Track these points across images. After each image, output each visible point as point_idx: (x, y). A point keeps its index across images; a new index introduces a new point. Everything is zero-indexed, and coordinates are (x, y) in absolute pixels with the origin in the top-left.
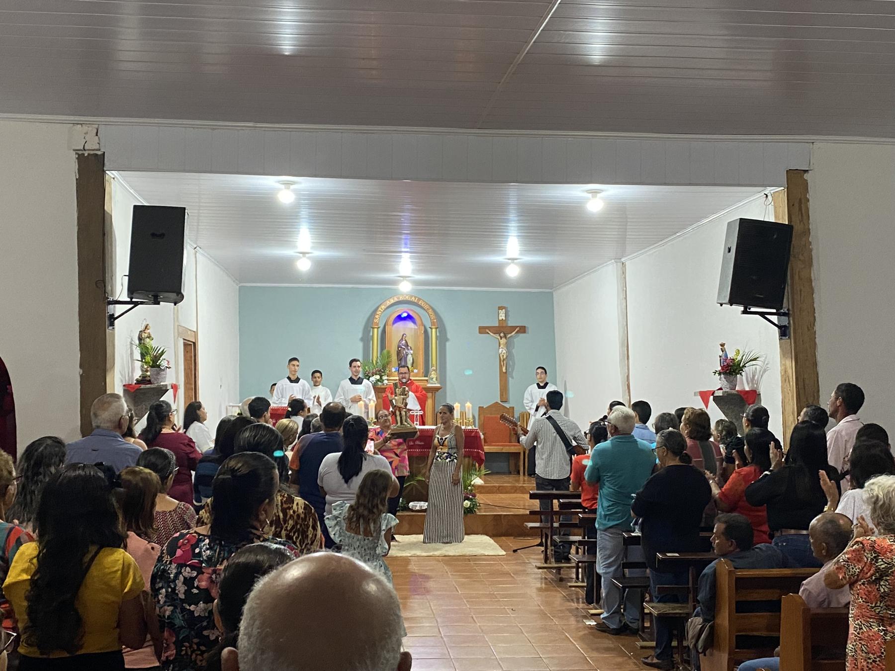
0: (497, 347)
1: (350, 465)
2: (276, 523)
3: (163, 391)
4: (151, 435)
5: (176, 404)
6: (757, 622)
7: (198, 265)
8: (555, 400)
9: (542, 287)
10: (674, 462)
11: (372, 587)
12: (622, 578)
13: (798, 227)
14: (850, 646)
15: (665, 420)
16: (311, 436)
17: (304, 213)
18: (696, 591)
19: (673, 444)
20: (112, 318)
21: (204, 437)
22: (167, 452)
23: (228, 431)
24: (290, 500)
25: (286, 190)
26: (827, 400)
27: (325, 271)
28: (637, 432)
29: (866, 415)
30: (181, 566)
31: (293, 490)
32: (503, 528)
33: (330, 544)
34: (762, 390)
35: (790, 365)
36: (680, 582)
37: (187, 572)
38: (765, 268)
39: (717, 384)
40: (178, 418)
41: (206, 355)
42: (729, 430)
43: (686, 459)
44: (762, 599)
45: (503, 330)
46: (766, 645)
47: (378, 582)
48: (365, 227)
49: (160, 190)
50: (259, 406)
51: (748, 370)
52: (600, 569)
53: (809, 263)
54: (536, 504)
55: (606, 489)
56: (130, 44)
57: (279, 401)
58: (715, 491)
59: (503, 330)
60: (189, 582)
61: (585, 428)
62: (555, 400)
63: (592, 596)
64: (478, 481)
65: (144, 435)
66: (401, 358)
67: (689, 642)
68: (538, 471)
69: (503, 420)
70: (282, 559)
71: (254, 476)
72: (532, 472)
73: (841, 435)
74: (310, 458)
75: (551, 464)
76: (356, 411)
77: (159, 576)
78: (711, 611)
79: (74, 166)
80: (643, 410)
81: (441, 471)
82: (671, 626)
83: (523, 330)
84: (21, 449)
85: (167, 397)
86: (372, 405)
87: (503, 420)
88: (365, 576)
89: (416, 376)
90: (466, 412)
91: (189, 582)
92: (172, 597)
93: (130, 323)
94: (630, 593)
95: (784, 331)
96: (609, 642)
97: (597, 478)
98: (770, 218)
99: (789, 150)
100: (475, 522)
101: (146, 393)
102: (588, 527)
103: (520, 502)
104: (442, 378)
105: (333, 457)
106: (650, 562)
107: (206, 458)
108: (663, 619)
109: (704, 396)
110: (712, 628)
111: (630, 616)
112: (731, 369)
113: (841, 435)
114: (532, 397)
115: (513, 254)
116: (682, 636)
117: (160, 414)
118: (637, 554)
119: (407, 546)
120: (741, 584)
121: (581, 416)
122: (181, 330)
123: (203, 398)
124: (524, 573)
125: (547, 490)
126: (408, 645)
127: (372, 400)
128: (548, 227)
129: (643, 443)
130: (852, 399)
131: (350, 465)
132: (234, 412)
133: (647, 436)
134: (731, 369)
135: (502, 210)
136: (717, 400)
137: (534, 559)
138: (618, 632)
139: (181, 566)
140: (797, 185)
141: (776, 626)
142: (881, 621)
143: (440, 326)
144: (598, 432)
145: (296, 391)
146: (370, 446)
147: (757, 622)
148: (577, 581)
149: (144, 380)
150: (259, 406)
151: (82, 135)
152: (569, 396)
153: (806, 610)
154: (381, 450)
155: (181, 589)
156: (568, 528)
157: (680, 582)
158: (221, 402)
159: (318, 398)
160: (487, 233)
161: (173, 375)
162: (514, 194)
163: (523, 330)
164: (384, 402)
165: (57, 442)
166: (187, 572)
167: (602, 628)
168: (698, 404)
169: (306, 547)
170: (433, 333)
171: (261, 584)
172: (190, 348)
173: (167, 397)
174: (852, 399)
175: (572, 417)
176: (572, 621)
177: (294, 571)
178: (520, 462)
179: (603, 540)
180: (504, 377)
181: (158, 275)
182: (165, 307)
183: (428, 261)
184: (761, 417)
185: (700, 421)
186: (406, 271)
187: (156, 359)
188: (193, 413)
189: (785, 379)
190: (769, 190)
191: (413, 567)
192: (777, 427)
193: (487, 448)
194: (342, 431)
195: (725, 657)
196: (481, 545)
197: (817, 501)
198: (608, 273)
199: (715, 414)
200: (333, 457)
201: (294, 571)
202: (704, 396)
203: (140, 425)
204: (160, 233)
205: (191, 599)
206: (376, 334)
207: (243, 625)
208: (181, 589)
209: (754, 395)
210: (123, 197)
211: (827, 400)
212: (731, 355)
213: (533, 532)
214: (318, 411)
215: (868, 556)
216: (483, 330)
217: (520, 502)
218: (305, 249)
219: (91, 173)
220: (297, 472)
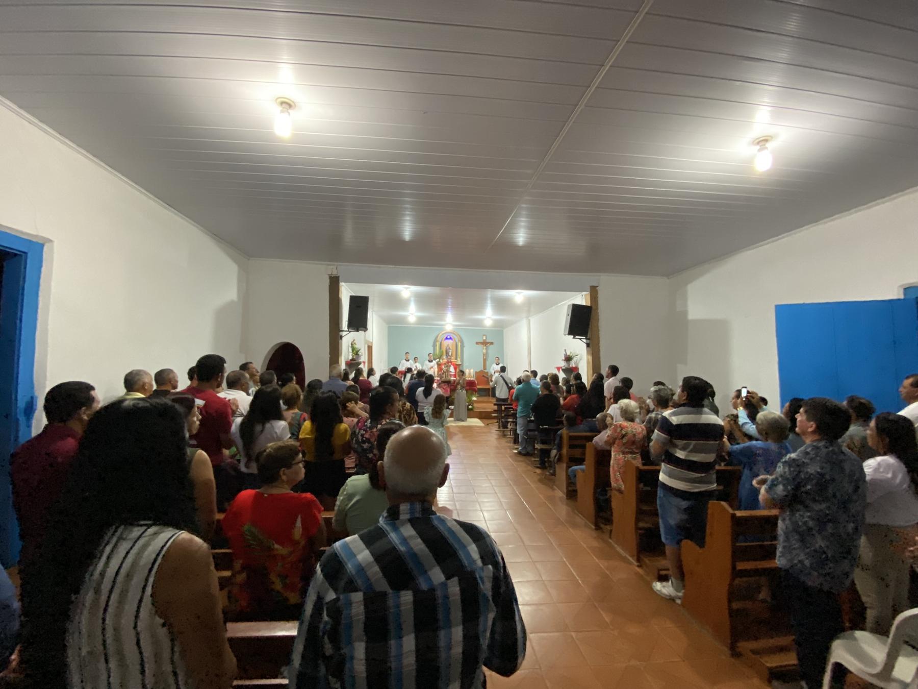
0: (482, 349)
1: (427, 393)
2: (400, 412)
3: (359, 364)
4: (356, 380)
5: (365, 368)
6: (577, 453)
7: (373, 318)
8: (503, 369)
9: (500, 329)
10: (546, 392)
11: (434, 439)
12: (526, 434)
13: (594, 307)
14: (612, 462)
15: (544, 377)
16: (413, 381)
17: (412, 299)
18: (554, 440)
19: (546, 386)
20: (341, 337)
21: (375, 381)
22: (364, 389)
23: (383, 379)
24: (405, 404)
25: (406, 291)
26: (605, 371)
27: (421, 320)
28: (532, 381)
29: (620, 376)
30: (360, 429)
31: (404, 400)
32: (483, 416)
33: (422, 420)
34: (580, 367)
35: (590, 358)
36: (549, 437)
37: (363, 432)
38: (581, 322)
39: (563, 364)
40: (365, 374)
41: (375, 350)
42: (567, 381)
43: (551, 391)
44: (578, 444)
45: (485, 343)
46: (580, 461)
47: (437, 437)
48: (434, 304)
49: (360, 290)
50: (394, 370)
51: (574, 359)
52: (518, 432)
53: (598, 320)
54: (496, 407)
55: (521, 402)
56: (349, 235)
57: (402, 368)
58: (562, 401)
59: (485, 343)
60: (362, 435)
61: (514, 379)
62: (503, 369)
63: (516, 441)
64: (474, 399)
65: (353, 380)
66: (447, 353)
67: (552, 459)
68: (497, 394)
69: (484, 376)
70: (400, 428)
71: (390, 396)
72: (494, 395)
73: (610, 384)
74: (413, 388)
75: (502, 393)
76: (430, 372)
77: (354, 434)
78: (560, 448)
79: (328, 281)
80: (535, 373)
81: (462, 393)
82: (545, 453)
83: (492, 343)
84: (307, 382)
85: (361, 366)
86: (436, 370)
87: (484, 376)
88: (431, 434)
89: (453, 360)
90: (470, 373)
91: (362, 435)
92: (357, 442)
93: (348, 338)
94: (530, 441)
95: (588, 345)
96: (522, 458)
97: (517, 399)
98: (584, 304)
99: (591, 279)
100: (471, 413)
101: (353, 364)
102: (514, 416)
103: (490, 406)
104: (462, 360)
105: (421, 389)
106: (537, 429)
107: (375, 389)
108: (541, 450)
109: (558, 369)
110: (560, 455)
111: (530, 449)
112: (568, 359)
113: (610, 384)
114: (494, 368)
115: (488, 317)
116: (549, 456)
117: (359, 372)
118: (532, 426)
119: (451, 422)
120: (571, 438)
121: (513, 375)
122: (366, 341)
123: (375, 366)
124: (490, 432)
125: (500, 402)
126: (448, 461)
127: (436, 368)
128: (502, 306)
129: (534, 385)
130: (614, 371)
131: (427, 393)
132: (386, 372)
133: (536, 383)
134: (568, 359)
135: (485, 299)
136: (564, 370)
137: (494, 429)
138: (525, 455)
139: (360, 429)
140: (594, 292)
141: (584, 454)
142: (624, 453)
143: (462, 342)
144: (519, 382)
145: (408, 365)
146: (435, 385)
147: (577, 453)
148: (510, 436)
149: (353, 360)
150: (394, 370)
151: (332, 269)
152: (508, 369)
153: (596, 448)
154: (439, 386)
155: (360, 438)
156: (508, 416)
157: (549, 437)
158: (381, 369)
159: (417, 367)
160: (479, 306)
161: (364, 358)
162: (490, 293)
163: (492, 343)
164: (440, 369)
165: (319, 381)
166: (363, 432)
167: (520, 453)
168: (555, 372)
169: (409, 423)
170: (459, 344)
171: (393, 437)
172: (370, 348)
173: (361, 366)
174: (614, 371)
175: (509, 376)
176: (508, 451)
177: (406, 432)
178: (491, 392)
179: (519, 421)
180: (485, 360)
181: (359, 321)
182: (361, 333)
183: (458, 318)
184: (578, 377)
185: (555, 378)
186: (449, 322)
187: (357, 352)
188: (371, 372)
189: (588, 362)
190: (584, 293)
191: (451, 430)
192: (585, 380)
193: (479, 387)
194: (424, 379)
195: (565, 465)
196: (475, 422)
197: (602, 408)
198: (525, 322)
199: (562, 376)
200: (421, 389)
201: (406, 432)
202: (558, 369)
203: (352, 376)
204: (359, 306)
205: (364, 442)
206: (438, 344)
207: (386, 452)
208: (360, 438)
209: (576, 369)
210: (346, 293)
211: (605, 371)
212: (568, 354)
213: (494, 418)
214: (415, 372)
215: (619, 430)
216: (477, 343)
217: (490, 406)
218: (412, 314)
219: (334, 283)
220: (408, 395)
